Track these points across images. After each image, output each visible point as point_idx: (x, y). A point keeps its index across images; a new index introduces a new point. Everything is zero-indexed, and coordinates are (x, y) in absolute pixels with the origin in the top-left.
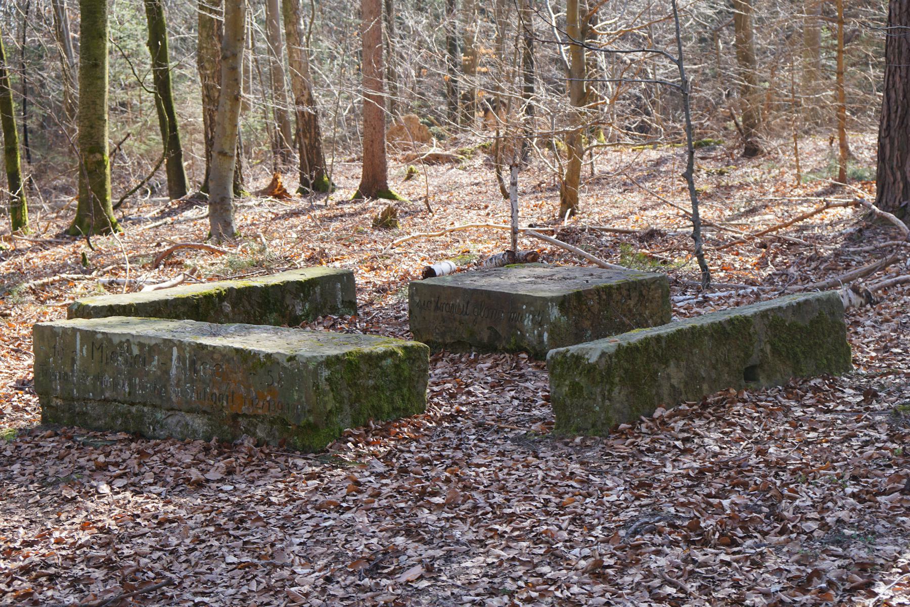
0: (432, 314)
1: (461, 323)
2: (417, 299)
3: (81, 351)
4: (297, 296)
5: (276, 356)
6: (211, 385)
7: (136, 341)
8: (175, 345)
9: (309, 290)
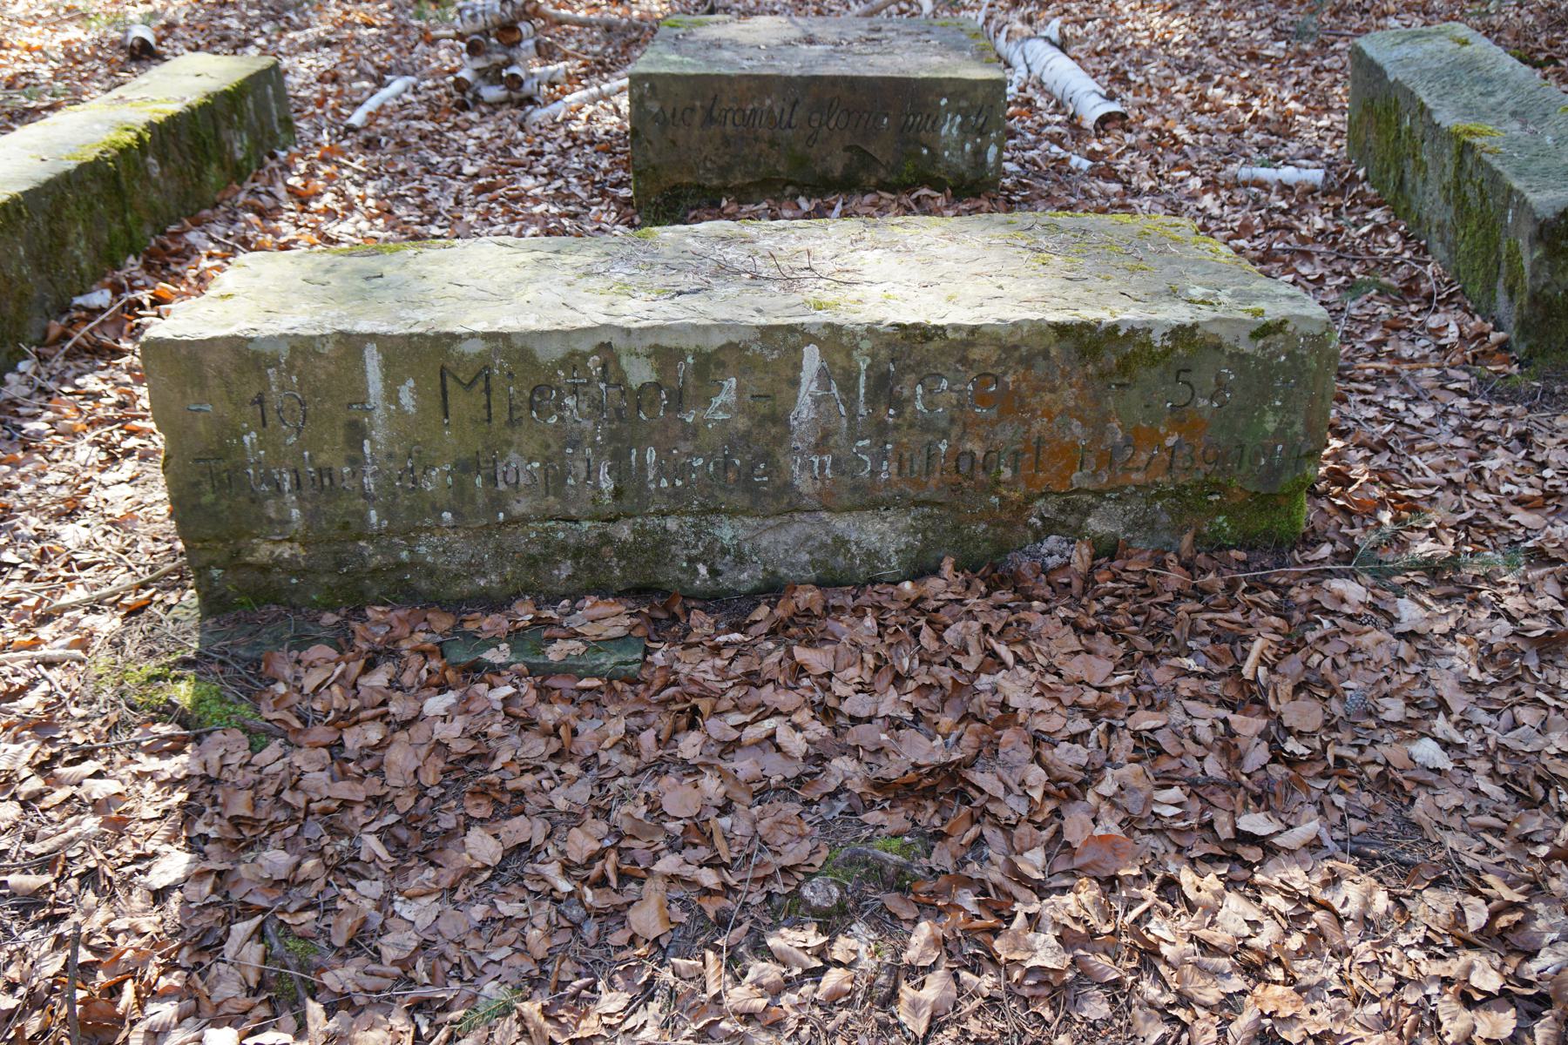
0: (696, 132)
1: (772, 143)
2: (654, 106)
3: (392, 396)
5: (1213, 329)
6: (956, 431)
7: (642, 345)
8: (810, 338)
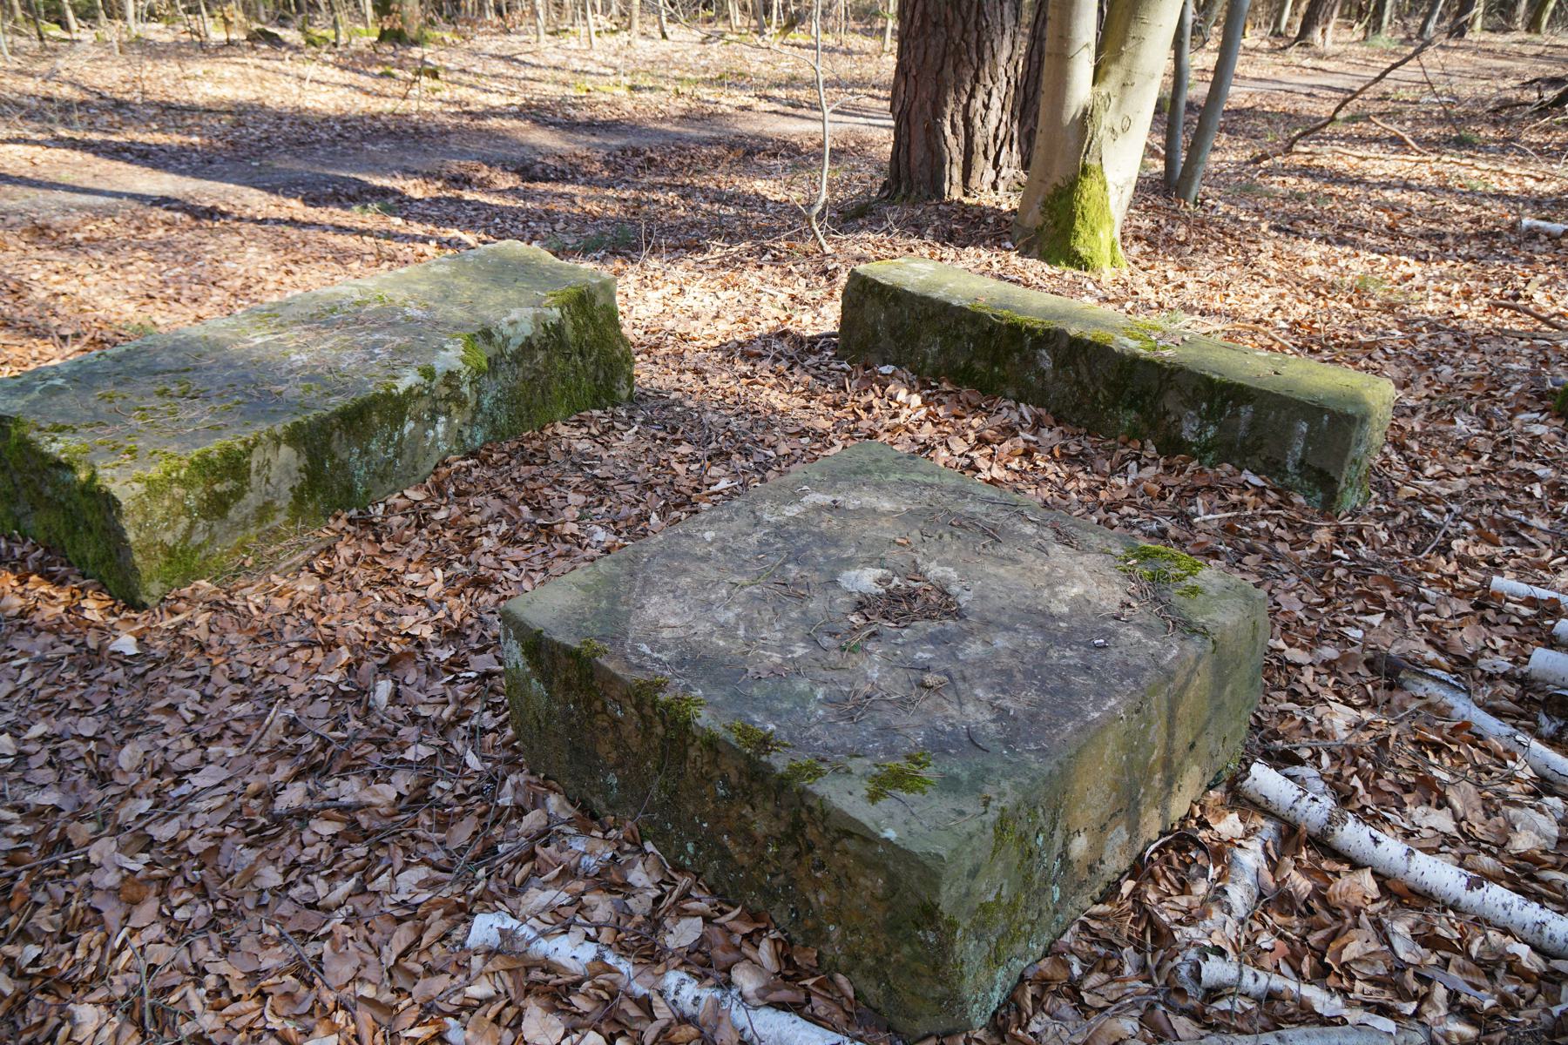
4: (1193, 403)
9: (1224, 401)
